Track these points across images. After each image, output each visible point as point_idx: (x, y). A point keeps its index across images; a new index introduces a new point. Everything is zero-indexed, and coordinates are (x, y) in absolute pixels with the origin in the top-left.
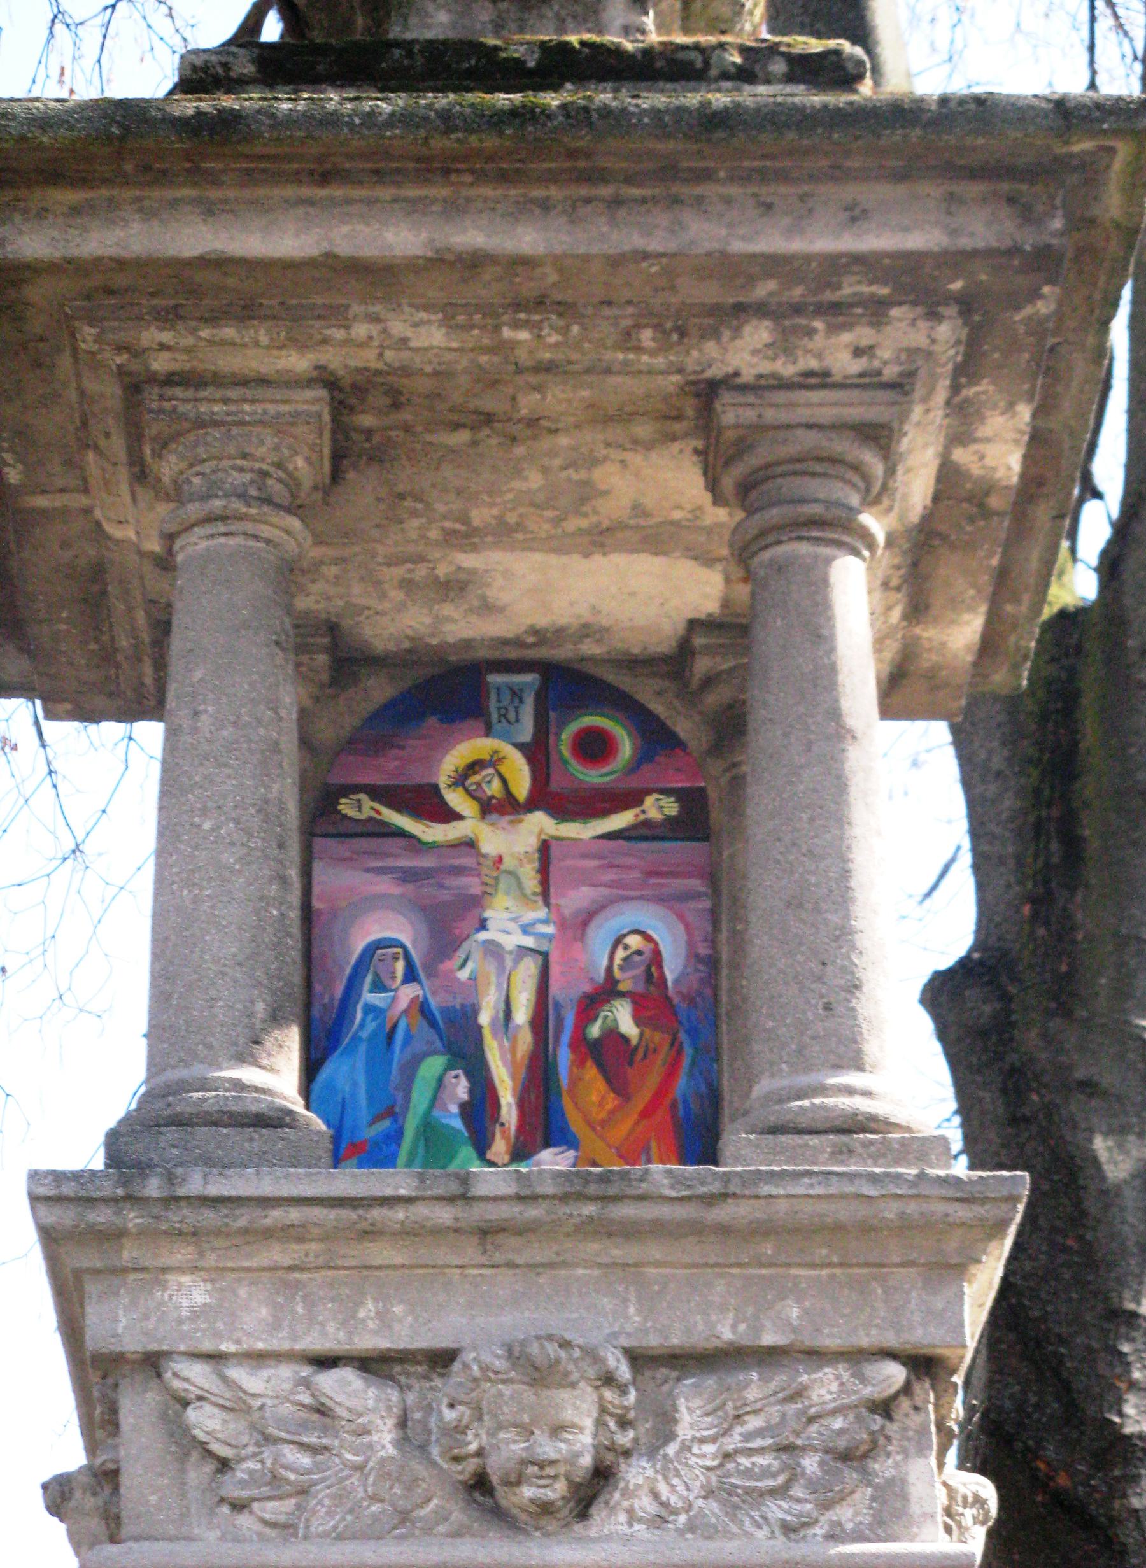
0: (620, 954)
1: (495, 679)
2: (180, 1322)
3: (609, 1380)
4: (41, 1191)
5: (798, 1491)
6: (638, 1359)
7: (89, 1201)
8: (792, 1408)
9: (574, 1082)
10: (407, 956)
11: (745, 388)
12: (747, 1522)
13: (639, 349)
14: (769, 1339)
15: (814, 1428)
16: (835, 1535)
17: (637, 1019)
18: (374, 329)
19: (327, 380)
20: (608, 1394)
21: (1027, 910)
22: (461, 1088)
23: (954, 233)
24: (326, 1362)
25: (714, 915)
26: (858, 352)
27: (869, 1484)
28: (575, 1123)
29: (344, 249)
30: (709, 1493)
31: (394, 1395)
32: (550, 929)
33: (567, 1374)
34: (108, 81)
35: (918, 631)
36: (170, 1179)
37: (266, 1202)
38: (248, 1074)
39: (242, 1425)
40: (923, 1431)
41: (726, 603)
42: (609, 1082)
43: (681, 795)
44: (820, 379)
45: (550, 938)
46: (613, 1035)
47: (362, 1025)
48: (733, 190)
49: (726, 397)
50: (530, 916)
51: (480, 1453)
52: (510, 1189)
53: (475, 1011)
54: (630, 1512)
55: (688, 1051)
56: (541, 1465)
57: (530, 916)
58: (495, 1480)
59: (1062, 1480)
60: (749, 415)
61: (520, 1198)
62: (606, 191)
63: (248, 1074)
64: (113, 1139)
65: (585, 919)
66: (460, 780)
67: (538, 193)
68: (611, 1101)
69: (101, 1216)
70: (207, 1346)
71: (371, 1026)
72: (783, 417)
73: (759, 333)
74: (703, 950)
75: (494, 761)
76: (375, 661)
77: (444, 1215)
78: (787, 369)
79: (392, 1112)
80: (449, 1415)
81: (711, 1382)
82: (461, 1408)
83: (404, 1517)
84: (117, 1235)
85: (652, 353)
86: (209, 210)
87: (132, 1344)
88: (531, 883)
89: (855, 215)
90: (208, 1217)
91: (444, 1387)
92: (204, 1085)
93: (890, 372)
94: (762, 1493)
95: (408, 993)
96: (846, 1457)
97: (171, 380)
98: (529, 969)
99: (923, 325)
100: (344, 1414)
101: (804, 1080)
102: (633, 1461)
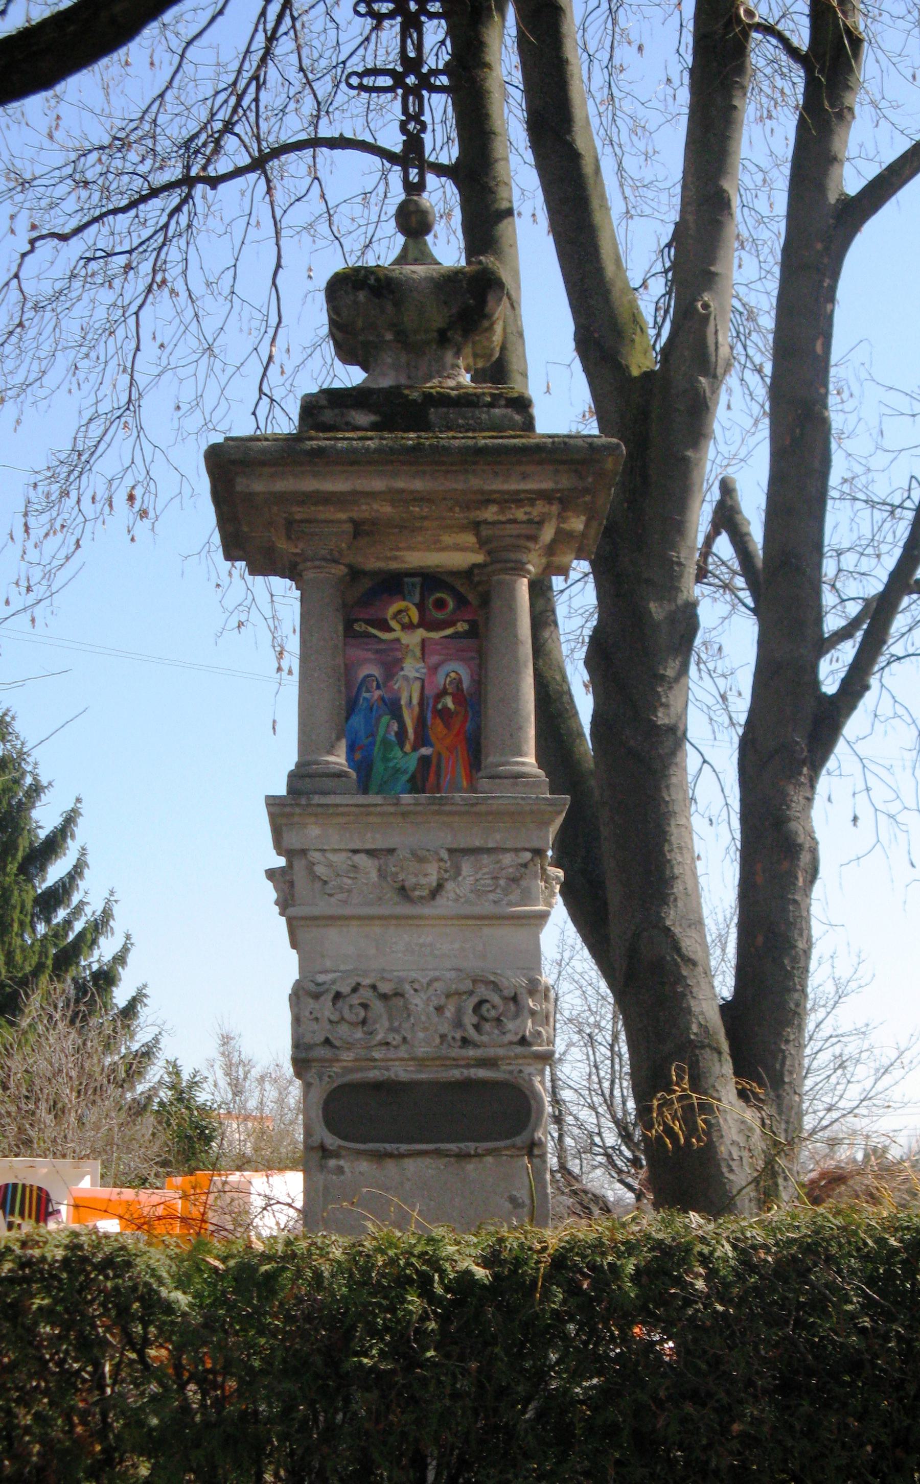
1: (406, 579)
3: (441, 860)
5: (498, 891)
6: (451, 851)
7: (284, 805)
11: (490, 523)
14: (490, 845)
16: (510, 904)
17: (454, 703)
19: (352, 520)
20: (442, 864)
21: (626, 505)
22: (395, 727)
23: (557, 483)
24: (355, 852)
25: (480, 666)
26: (526, 513)
28: (433, 739)
29: (359, 488)
30: (472, 891)
31: (376, 862)
34: (243, 194)
35: (553, 559)
36: (308, 799)
37: (337, 805)
38: (331, 759)
40: (536, 872)
44: (514, 521)
46: (446, 709)
48: (485, 468)
49: (482, 527)
52: (412, 802)
53: (399, 700)
55: (470, 714)
59: (632, 743)
60: (490, 532)
61: (415, 804)
62: (443, 468)
63: (331, 759)
67: (421, 468)
68: (445, 731)
69: (287, 810)
71: (365, 705)
73: (493, 508)
74: (476, 678)
75: (406, 610)
76: (365, 573)
77: (391, 809)
78: (502, 518)
79: (373, 735)
80: (393, 869)
81: (472, 858)
83: (380, 899)
84: (291, 815)
86: (315, 475)
88: (418, 653)
89: (524, 477)
90: (320, 810)
91: (392, 860)
92: (317, 763)
93: (536, 519)
95: (377, 693)
97: (302, 521)
98: (417, 686)
99: (547, 506)
101: (503, 759)
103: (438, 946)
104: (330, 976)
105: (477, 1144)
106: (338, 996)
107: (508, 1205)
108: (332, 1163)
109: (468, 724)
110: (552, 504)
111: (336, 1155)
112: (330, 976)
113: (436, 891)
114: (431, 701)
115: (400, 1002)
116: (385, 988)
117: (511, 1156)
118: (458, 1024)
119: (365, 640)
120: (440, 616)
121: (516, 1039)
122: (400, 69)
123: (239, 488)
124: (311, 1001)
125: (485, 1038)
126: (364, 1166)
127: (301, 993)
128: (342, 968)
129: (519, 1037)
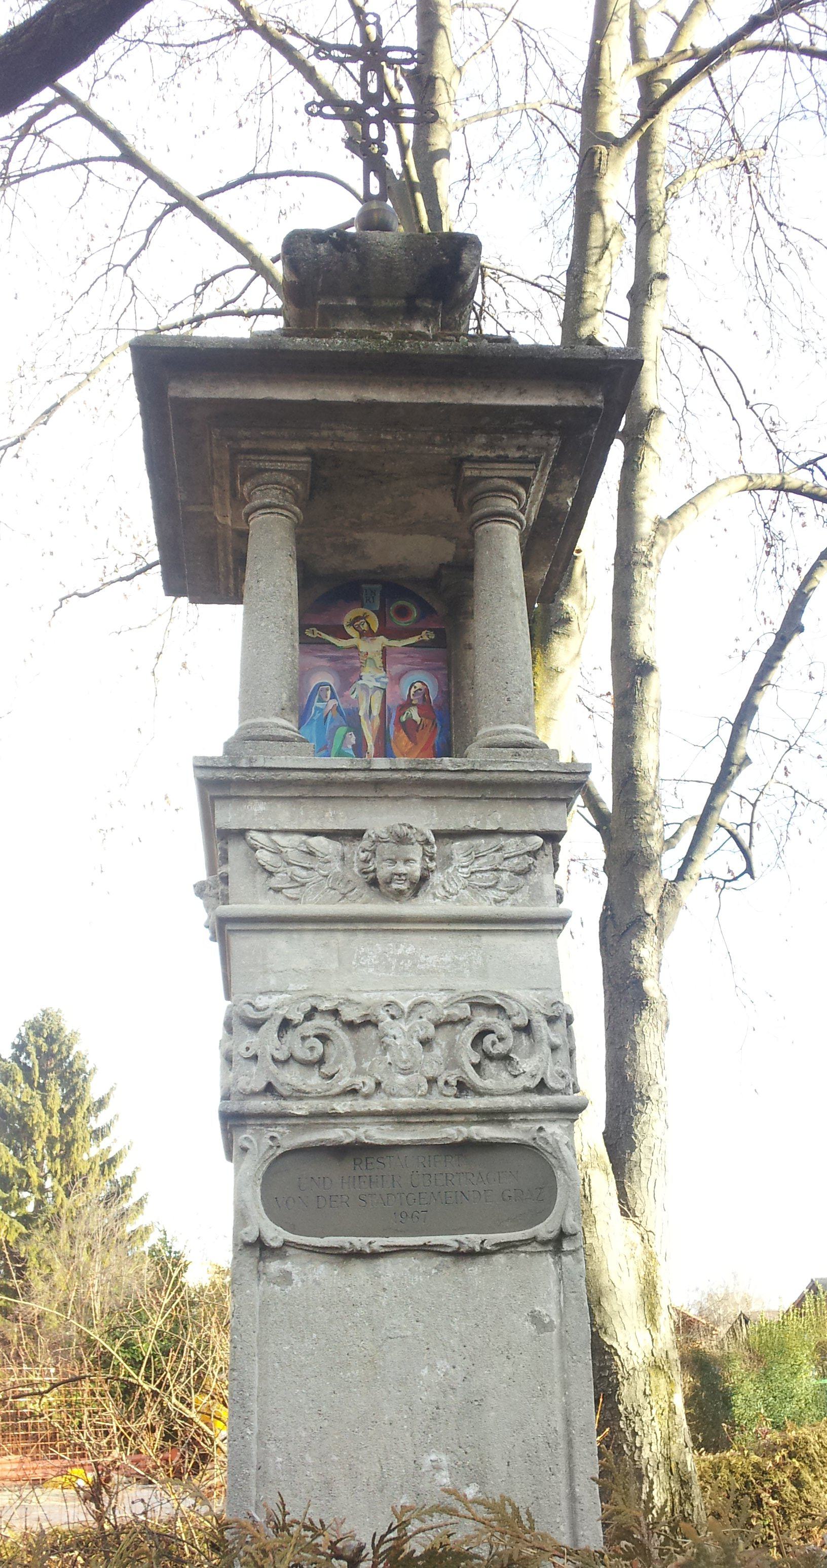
0: (413, 690)
1: (363, 586)
2: (254, 818)
4: (199, 764)
5: (500, 887)
8: (498, 855)
9: (395, 737)
10: (332, 690)
12: (480, 899)
13: (434, 445)
15: (506, 862)
18: (331, 433)
22: (353, 739)
25: (449, 676)
27: (528, 884)
32: (386, 680)
33: (411, 839)
39: (278, 858)
41: (455, 557)
42: (409, 737)
43: (435, 631)
45: (386, 684)
46: (410, 720)
47: (314, 715)
50: (378, 675)
51: (375, 870)
54: (434, 894)
56: (400, 875)
57: (378, 675)
58: (380, 881)
60: (476, 473)
64: (227, 744)
65: (399, 678)
66: (352, 624)
68: (410, 745)
70: (265, 827)
71: (318, 715)
72: (490, 474)
75: (364, 617)
78: (490, 454)
82: (367, 853)
85: (439, 446)
87: (234, 826)
88: (379, 662)
89: (521, 392)
94: (486, 888)
95: (332, 703)
96: (518, 874)
98: (378, 695)
100: (320, 855)
102: (435, 873)
103: (422, 958)
104: (275, 999)
105: (484, 1236)
106: (286, 1025)
107: (530, 1328)
108: (274, 1266)
109: (437, 738)
110: (550, 435)
111: (279, 1252)
112: (275, 999)
113: (419, 884)
114: (394, 714)
115: (370, 1034)
116: (350, 1014)
117: (531, 1253)
118: (453, 1063)
119: (320, 646)
120: (403, 623)
121: (533, 1084)
122: (360, 102)
123: (172, 393)
124: (247, 1032)
125: (488, 1083)
126: (321, 1270)
127: (235, 1022)
128: (292, 987)
129: (537, 1081)
